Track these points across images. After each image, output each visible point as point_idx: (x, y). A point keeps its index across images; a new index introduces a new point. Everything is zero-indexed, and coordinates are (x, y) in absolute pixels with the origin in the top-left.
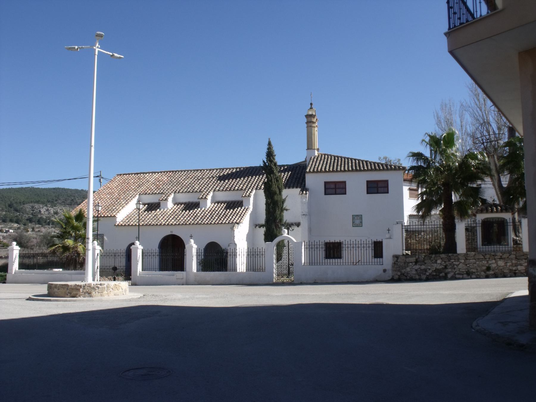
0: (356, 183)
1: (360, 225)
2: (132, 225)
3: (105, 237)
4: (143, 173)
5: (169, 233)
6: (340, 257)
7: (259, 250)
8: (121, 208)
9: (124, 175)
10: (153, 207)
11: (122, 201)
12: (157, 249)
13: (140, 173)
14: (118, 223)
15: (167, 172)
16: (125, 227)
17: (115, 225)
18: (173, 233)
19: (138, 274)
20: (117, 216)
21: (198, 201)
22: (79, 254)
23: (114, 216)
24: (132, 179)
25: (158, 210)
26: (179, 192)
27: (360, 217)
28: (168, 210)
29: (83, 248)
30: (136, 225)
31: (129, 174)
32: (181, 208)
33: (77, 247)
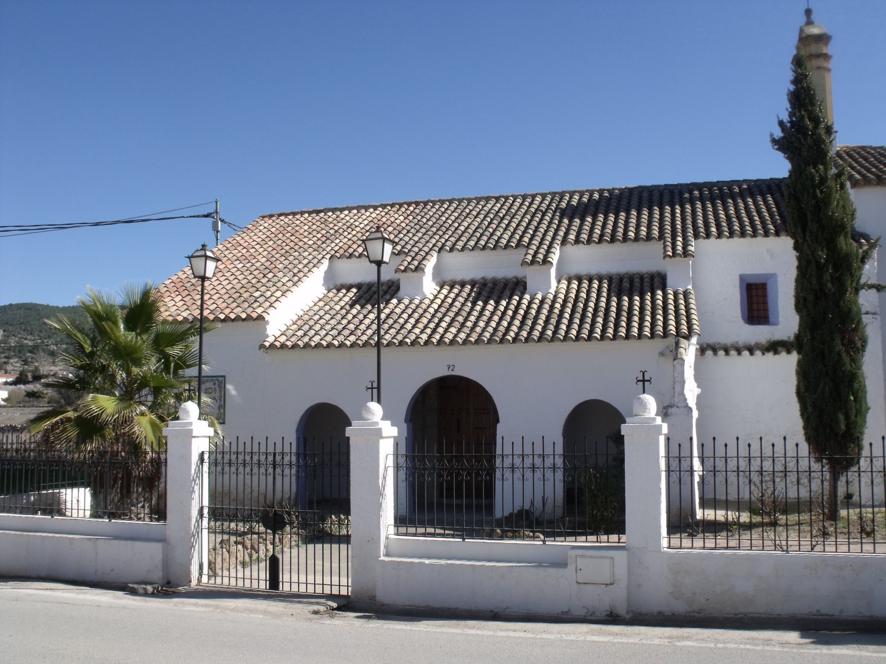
2: (319, 345)
3: (230, 387)
4: (333, 210)
5: (443, 372)
6: (620, 529)
7: (720, 452)
8: (278, 294)
9: (280, 215)
10: (375, 294)
11: (280, 275)
12: (291, 437)
13: (325, 211)
14: (271, 339)
15: (401, 205)
16: (296, 352)
17: (262, 346)
18: (457, 372)
20: (267, 317)
21: (396, 276)
22: (135, 447)
23: (260, 318)
24: (304, 224)
25: (394, 301)
26: (452, 249)
28: (427, 301)
29: (153, 425)
30: (366, 344)
31: (294, 214)
32: (347, 299)
33: (128, 421)
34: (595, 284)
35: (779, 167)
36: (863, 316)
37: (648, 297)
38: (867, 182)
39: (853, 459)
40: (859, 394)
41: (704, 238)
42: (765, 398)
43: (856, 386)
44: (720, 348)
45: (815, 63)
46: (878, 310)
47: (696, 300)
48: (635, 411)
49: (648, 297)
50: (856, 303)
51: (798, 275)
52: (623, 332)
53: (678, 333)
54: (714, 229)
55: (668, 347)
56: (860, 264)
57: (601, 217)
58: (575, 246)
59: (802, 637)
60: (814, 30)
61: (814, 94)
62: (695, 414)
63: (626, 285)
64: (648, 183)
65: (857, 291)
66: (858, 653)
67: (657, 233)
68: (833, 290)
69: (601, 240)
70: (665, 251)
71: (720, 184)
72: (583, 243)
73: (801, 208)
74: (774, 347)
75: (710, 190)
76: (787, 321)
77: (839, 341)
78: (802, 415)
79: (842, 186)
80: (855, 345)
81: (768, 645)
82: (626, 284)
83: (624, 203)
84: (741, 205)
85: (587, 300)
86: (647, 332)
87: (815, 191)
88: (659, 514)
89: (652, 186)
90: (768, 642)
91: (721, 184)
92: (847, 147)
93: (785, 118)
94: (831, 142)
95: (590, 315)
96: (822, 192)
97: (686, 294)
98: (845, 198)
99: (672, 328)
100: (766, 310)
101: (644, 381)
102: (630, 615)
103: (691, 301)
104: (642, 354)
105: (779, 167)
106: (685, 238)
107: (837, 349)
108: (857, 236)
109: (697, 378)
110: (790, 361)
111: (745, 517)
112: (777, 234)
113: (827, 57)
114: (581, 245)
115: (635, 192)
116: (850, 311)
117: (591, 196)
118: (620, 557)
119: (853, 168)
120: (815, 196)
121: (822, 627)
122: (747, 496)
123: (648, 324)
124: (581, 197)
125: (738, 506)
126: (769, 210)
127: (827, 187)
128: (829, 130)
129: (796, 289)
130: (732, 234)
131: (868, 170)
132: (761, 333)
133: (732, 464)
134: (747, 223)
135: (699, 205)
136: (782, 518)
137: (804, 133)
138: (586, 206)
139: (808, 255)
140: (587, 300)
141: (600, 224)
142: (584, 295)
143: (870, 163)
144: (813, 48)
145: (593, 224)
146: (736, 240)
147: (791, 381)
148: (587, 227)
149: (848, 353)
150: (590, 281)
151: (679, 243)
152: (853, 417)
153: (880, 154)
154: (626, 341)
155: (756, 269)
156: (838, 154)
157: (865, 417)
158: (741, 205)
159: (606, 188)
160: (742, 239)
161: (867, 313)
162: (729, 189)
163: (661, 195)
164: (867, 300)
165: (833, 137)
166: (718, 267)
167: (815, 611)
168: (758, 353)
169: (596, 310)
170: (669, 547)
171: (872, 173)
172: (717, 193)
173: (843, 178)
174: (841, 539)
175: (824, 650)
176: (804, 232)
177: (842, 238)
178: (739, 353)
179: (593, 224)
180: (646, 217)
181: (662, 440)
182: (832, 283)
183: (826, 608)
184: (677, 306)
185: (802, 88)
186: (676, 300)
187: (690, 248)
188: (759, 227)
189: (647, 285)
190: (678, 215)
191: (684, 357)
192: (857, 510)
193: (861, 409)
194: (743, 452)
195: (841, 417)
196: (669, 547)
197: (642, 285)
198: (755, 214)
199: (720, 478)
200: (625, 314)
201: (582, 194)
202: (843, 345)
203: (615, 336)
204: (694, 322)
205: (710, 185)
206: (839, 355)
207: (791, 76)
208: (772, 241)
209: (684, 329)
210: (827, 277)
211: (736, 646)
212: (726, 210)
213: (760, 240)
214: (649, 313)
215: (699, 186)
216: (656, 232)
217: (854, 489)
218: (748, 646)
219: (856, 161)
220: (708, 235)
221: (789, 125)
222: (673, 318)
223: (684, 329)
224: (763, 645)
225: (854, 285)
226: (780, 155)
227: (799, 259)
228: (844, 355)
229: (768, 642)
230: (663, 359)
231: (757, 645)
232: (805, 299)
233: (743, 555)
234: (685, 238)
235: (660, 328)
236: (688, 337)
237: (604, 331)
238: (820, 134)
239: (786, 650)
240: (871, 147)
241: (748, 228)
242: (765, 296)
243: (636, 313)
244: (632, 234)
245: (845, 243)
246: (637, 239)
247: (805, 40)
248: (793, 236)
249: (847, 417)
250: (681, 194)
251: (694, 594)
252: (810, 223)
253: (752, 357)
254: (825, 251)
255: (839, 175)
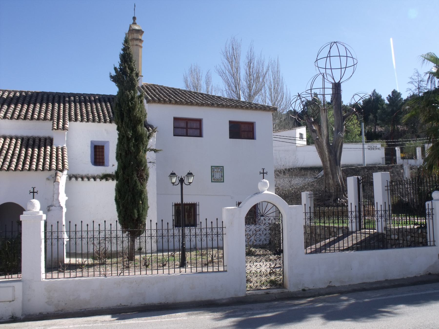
0: (216, 122)
1: (221, 180)
7: (85, 228)
19: (387, 102)
27: (221, 168)
34: (14, 141)
35: (113, 90)
36: (147, 164)
37: (43, 149)
38: (154, 101)
39: (141, 231)
40: (144, 201)
41: (74, 121)
42: (100, 201)
43: (143, 196)
44: (79, 177)
45: (136, 42)
46: (155, 161)
47: (68, 152)
48: (28, 208)
49: (43, 149)
50: (144, 157)
51: (118, 143)
52: (27, 167)
53: (57, 168)
54: (79, 117)
55: (51, 176)
56: (147, 139)
57: (20, 106)
58: (3, 120)
59: (112, 317)
60: (136, 27)
61: (132, 57)
62: (65, 210)
63: (30, 142)
64: (48, 91)
65: (145, 151)
66: (137, 322)
67: (50, 117)
68: (134, 151)
69: (18, 118)
70: (53, 126)
71: (84, 95)
72: (8, 118)
73: (122, 110)
74: (106, 177)
75: (79, 97)
76: (112, 165)
77: (136, 175)
78: (117, 210)
79: (141, 102)
80: (143, 177)
81: (95, 323)
82: (31, 142)
83: (33, 99)
84: (94, 106)
85: (8, 149)
86: (40, 167)
87: (129, 103)
88: (40, 262)
89: (49, 92)
90: (96, 322)
91: (85, 95)
92: (147, 84)
93: (118, 66)
94: (138, 80)
95: (9, 157)
96: (132, 103)
97: (62, 149)
98: (142, 107)
99: (54, 166)
100: (103, 159)
101: (34, 192)
102: (24, 317)
103: (65, 152)
104: (37, 179)
105: (113, 90)
106: (64, 120)
107: (135, 179)
108: (147, 126)
109: (67, 192)
110: (112, 184)
111: (90, 261)
112: (110, 122)
113: (141, 41)
114: (7, 120)
115: (40, 95)
116: (141, 161)
117: (15, 94)
118: (18, 286)
119: (148, 94)
120: (128, 105)
121: (121, 312)
122: (109, 249)
123: (41, 163)
124: (9, 94)
125: (87, 256)
126: (108, 110)
127: (135, 101)
128: (137, 75)
129: (117, 149)
130: (88, 120)
131: (155, 96)
132: (100, 170)
133: (79, 235)
134: (96, 116)
135: (73, 104)
136: (108, 261)
137: (126, 74)
138: (12, 99)
139: (123, 133)
140: (8, 149)
141: (19, 109)
142: (7, 147)
143: (156, 93)
144: (135, 36)
145: (15, 109)
146: (90, 123)
147: (113, 194)
148: (11, 110)
149: (140, 181)
150: (11, 139)
151: (61, 123)
152: (141, 212)
153: (161, 89)
154: (29, 172)
155: (99, 138)
156: (142, 87)
157: (147, 211)
158: (94, 106)
159: (24, 91)
160: (93, 123)
161: (150, 162)
162: (89, 98)
163: (54, 97)
164: (150, 156)
165: (139, 78)
166: (82, 136)
167: (119, 304)
168: (98, 180)
169: (13, 155)
170: (46, 279)
171: (156, 97)
172: (83, 99)
173: (142, 98)
174: (137, 269)
175: (122, 322)
176: (122, 122)
177: (140, 126)
178: (89, 180)
179: (15, 109)
180: (44, 108)
181: (43, 223)
182: (134, 147)
183: (125, 302)
184: (57, 155)
185: (127, 53)
186: (57, 152)
187: (66, 126)
188: (102, 118)
189: (42, 143)
190: (62, 108)
191: (59, 181)
192: (144, 255)
193: (145, 208)
194: (209, 225)
195: (136, 211)
196: (46, 279)
197: (40, 143)
198: (101, 111)
199: (165, 239)
200: (29, 157)
201: (10, 92)
202: (138, 177)
203: (23, 169)
204: (66, 163)
205: (79, 95)
206: (136, 182)
207: (122, 47)
208: (108, 125)
209: (60, 166)
210: (131, 144)
211: (79, 325)
212: (86, 108)
213: (102, 124)
214: (42, 158)
215: (74, 95)
216: (49, 116)
217: (143, 245)
218: (85, 325)
219: (150, 91)
220: (76, 120)
221: (119, 70)
222: (55, 161)
223: (60, 166)
224: (93, 323)
225: (144, 149)
226: (114, 84)
227: (119, 135)
228: (138, 182)
229: (96, 322)
230: (48, 181)
231: (90, 324)
232: (121, 154)
233: (84, 280)
234: (64, 120)
235: (47, 166)
236: (62, 171)
237: (17, 166)
238: (133, 76)
239: (104, 324)
240: (157, 85)
241: (97, 118)
242: (103, 152)
243: (35, 157)
244: (36, 116)
245: (141, 129)
246: (39, 119)
247: (132, 31)
248: (117, 123)
249: (138, 211)
250: (64, 98)
251: (59, 301)
252: (125, 118)
253: (77, 182)
254: (131, 132)
255: (140, 96)
